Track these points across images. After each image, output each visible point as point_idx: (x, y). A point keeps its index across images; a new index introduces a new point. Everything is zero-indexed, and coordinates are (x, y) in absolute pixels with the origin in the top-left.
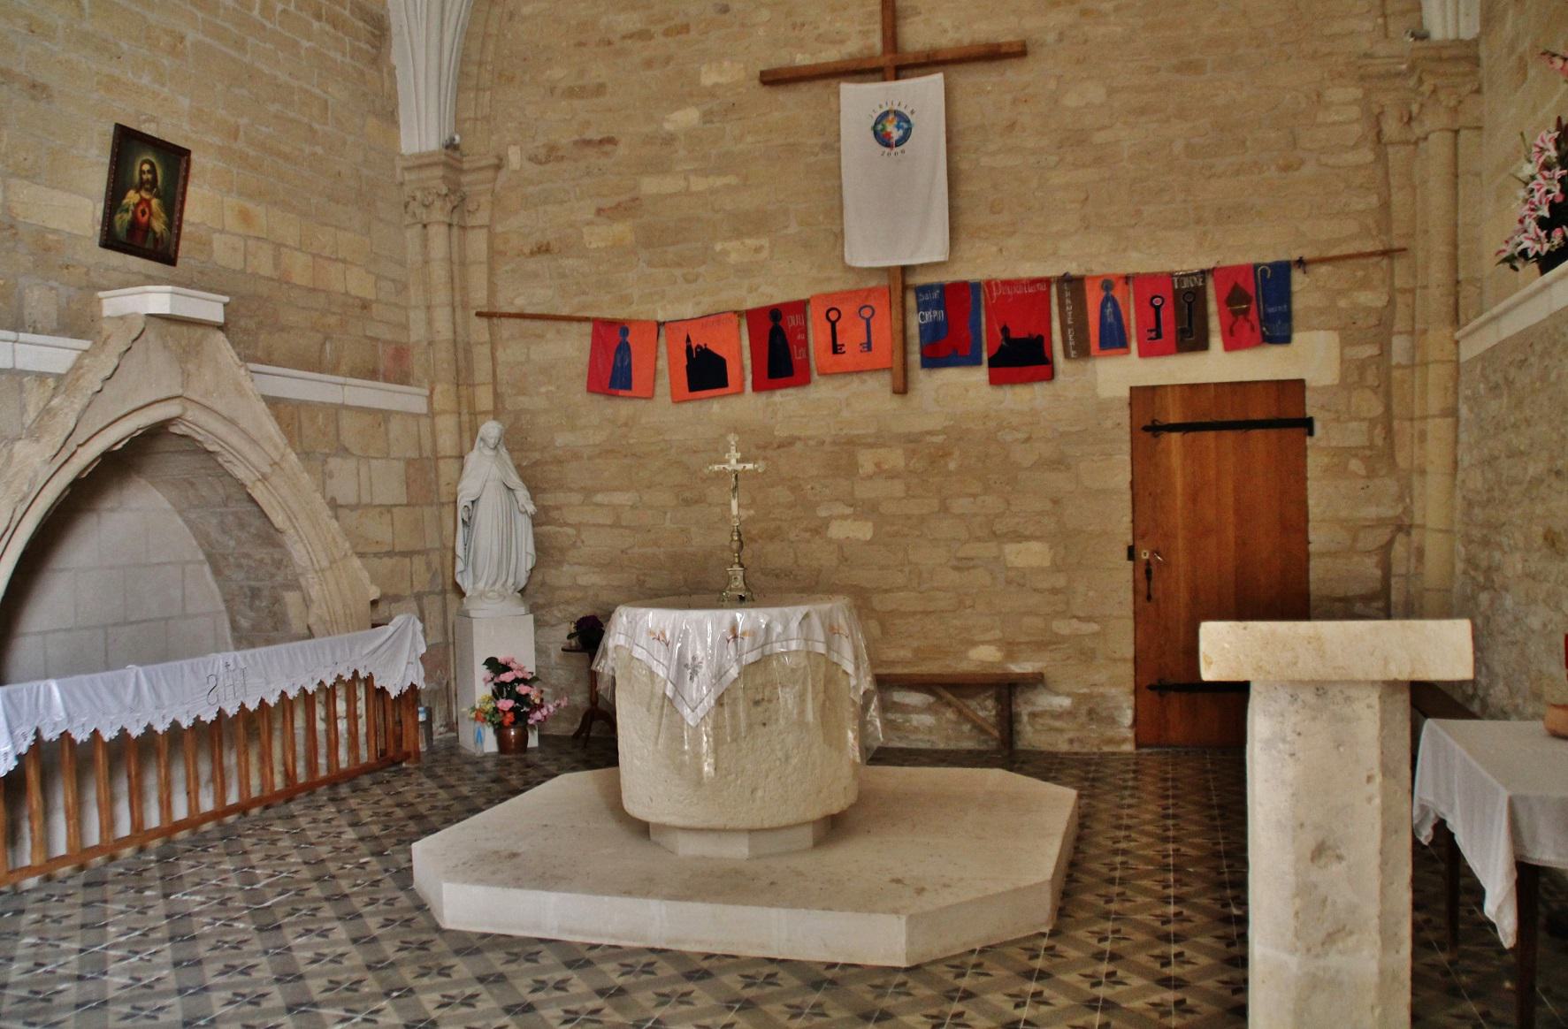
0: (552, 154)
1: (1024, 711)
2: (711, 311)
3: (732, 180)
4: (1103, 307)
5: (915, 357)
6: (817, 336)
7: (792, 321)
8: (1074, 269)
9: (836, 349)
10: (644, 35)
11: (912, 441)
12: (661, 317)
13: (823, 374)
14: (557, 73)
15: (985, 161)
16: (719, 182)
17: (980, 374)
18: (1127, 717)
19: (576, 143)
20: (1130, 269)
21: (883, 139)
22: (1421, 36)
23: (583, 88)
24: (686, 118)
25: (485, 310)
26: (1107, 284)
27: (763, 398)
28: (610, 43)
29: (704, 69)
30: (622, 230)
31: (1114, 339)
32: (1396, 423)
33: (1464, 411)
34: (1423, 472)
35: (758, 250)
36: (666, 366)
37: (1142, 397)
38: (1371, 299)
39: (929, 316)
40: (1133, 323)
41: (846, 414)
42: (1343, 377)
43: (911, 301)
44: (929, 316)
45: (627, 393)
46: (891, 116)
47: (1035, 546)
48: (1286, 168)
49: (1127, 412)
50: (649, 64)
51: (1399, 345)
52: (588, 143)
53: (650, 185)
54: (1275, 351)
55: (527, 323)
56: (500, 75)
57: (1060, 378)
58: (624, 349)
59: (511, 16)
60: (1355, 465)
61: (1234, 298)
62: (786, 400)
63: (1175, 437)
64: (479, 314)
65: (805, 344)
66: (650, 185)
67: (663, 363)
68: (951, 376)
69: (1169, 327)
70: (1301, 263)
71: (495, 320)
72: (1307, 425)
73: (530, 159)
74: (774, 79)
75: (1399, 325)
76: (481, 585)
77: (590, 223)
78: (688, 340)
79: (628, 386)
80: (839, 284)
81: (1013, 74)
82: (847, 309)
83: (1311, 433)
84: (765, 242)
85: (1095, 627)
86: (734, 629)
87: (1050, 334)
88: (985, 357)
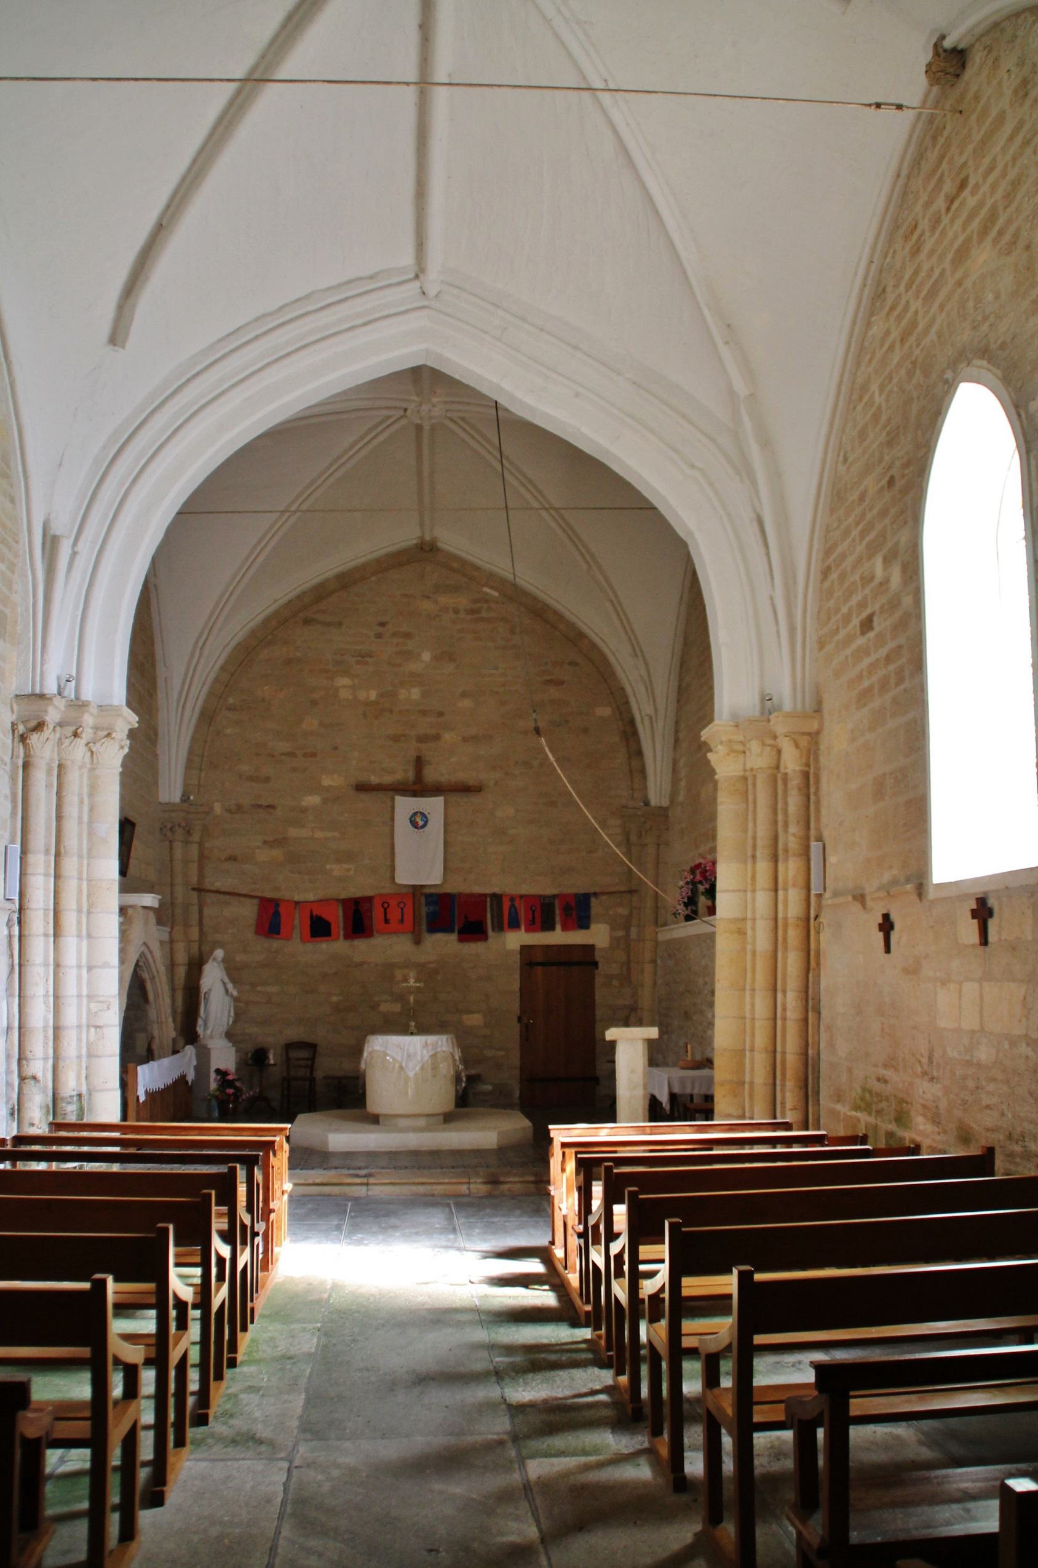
3: (337, 834)
4: (510, 908)
5: (424, 927)
6: (377, 913)
8: (497, 890)
9: (387, 921)
10: (292, 755)
11: (421, 967)
12: (297, 898)
13: (378, 932)
14: (245, 768)
16: (329, 834)
17: (454, 937)
18: (517, 1094)
20: (523, 892)
21: (414, 824)
22: (647, 803)
24: (313, 800)
25: (196, 886)
26: (512, 899)
27: (348, 943)
28: (273, 756)
29: (324, 777)
30: (277, 853)
31: (514, 925)
33: (659, 962)
34: (642, 986)
35: (348, 870)
36: (298, 923)
37: (525, 949)
38: (623, 911)
39: (432, 908)
40: (523, 913)
43: (423, 900)
44: (432, 908)
45: (278, 936)
46: (419, 814)
47: (476, 1016)
48: (590, 852)
49: (519, 956)
50: (294, 770)
51: (634, 931)
52: (260, 806)
53: (293, 832)
54: (583, 932)
55: (222, 896)
56: (211, 763)
57: (490, 940)
58: (277, 914)
60: (615, 982)
61: (567, 909)
63: (540, 968)
64: (194, 889)
65: (371, 917)
66: (293, 832)
67: (297, 922)
68: (440, 937)
69: (538, 920)
70: (595, 894)
71: (203, 893)
72: (595, 964)
73: (226, 810)
74: (362, 788)
75: (635, 921)
76: (209, 1032)
77: (258, 847)
78: (311, 912)
79: (278, 933)
80: (388, 889)
81: (475, 799)
83: (597, 968)
84: (351, 866)
86: (426, 1043)
87: (486, 919)
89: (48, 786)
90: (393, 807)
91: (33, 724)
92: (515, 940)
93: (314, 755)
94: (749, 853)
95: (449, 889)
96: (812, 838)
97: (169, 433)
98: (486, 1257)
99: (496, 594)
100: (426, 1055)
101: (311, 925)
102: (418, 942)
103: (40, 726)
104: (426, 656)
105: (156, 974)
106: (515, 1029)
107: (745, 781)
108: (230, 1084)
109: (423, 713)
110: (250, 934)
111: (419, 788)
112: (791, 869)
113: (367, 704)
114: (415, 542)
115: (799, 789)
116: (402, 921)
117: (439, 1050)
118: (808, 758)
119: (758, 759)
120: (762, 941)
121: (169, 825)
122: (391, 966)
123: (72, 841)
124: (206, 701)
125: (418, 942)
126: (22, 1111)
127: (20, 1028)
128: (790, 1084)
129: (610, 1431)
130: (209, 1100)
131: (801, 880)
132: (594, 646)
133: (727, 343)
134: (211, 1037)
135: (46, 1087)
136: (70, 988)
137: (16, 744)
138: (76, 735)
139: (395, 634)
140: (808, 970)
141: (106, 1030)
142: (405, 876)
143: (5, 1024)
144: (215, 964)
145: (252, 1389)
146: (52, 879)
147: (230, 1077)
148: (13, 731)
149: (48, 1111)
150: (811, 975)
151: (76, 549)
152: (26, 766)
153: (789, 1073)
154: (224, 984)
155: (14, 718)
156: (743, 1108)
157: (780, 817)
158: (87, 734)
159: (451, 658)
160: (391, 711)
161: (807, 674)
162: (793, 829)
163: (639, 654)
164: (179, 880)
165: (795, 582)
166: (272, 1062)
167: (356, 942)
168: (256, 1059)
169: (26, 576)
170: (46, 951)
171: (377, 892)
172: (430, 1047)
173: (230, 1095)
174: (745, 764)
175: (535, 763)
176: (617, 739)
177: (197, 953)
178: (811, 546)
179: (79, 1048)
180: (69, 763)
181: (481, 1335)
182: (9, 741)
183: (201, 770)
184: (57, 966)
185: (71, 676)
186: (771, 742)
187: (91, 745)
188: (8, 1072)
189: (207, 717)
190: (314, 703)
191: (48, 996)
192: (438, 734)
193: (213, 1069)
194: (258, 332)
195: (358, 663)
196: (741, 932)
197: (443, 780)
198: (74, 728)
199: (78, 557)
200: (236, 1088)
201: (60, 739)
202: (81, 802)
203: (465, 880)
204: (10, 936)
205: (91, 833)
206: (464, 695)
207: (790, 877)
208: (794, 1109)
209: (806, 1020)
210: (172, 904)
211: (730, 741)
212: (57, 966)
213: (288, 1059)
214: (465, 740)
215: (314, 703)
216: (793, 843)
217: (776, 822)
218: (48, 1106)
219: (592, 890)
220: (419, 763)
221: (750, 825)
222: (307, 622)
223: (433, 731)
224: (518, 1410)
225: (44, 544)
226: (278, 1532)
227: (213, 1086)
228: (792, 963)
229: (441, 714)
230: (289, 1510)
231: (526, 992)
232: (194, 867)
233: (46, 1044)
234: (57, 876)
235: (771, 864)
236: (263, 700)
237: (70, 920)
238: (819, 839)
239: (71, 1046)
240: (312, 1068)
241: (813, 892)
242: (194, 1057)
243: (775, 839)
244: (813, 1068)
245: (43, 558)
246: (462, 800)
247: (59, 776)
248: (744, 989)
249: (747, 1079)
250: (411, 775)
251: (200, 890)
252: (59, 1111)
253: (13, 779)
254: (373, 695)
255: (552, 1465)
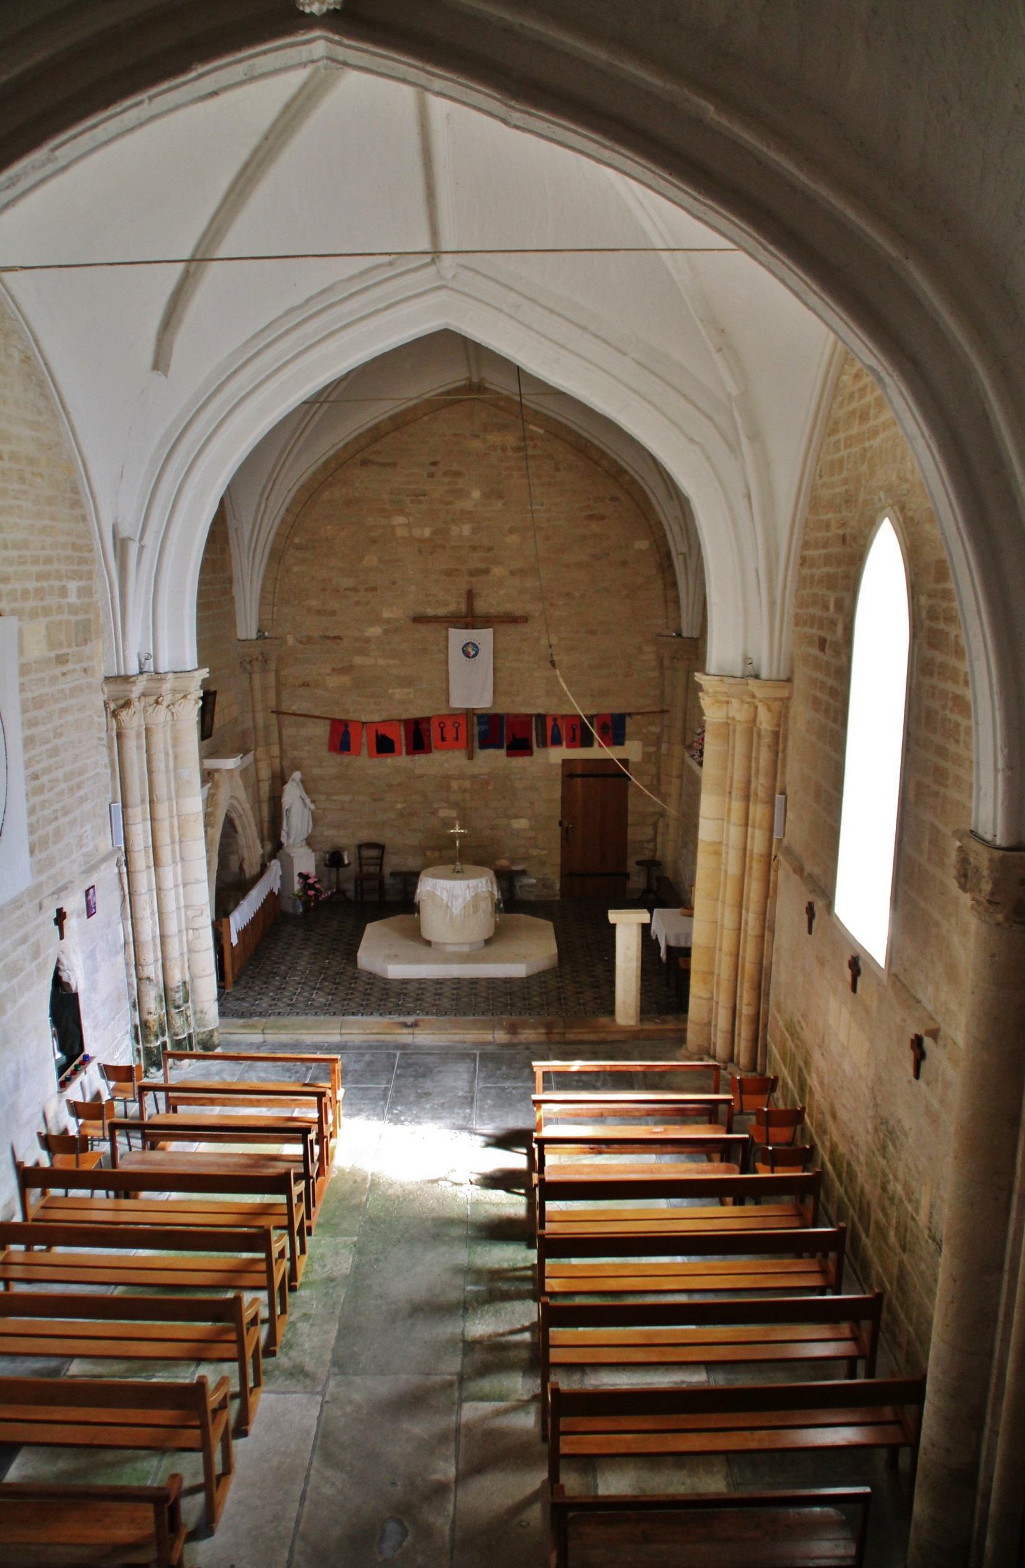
0: (310, 640)
1: (518, 884)
2: (387, 719)
4: (553, 728)
5: (476, 744)
6: (435, 733)
7: (424, 726)
8: (541, 711)
9: (443, 739)
10: (355, 590)
11: (473, 778)
12: (364, 719)
13: (437, 748)
14: (313, 603)
15: (507, 664)
16: (391, 662)
17: (503, 752)
18: (558, 886)
19: (321, 637)
20: (564, 712)
21: (466, 654)
22: (679, 635)
23: (325, 611)
24: (375, 631)
26: (555, 719)
27: (409, 758)
28: (338, 591)
30: (345, 680)
31: (556, 742)
32: (662, 776)
34: (670, 796)
35: (408, 694)
36: (365, 740)
37: (566, 763)
38: (655, 729)
39: (483, 728)
41: (446, 765)
42: (643, 759)
43: (475, 720)
44: (483, 728)
50: (357, 603)
51: (664, 746)
52: (327, 638)
53: (358, 660)
55: (298, 718)
57: (535, 754)
59: (287, 571)
62: (421, 759)
63: (579, 779)
64: (273, 712)
65: (430, 736)
66: (358, 660)
67: (364, 740)
70: (630, 714)
74: (420, 619)
75: (665, 738)
76: (291, 841)
77: (328, 675)
78: (377, 731)
80: (444, 712)
82: (449, 723)
84: (411, 690)
85: (546, 852)
88: (505, 746)
89: (139, 748)
90: (447, 637)
91: (121, 702)
92: (558, 754)
93: (374, 589)
94: (728, 790)
95: (498, 710)
96: (778, 790)
97: (214, 426)
98: (488, 1145)
99: (542, 432)
100: (469, 895)
101: (377, 743)
102: (471, 756)
103: (127, 704)
104: (476, 494)
105: (242, 812)
106: (557, 832)
107: (727, 726)
108: (312, 887)
109: (474, 548)
110: (324, 752)
111: (470, 620)
112: (758, 811)
113: (421, 541)
114: (463, 383)
115: (769, 747)
116: (457, 739)
117: (479, 891)
118: (779, 719)
119: (738, 712)
120: (732, 867)
121: (248, 659)
122: (448, 778)
123: (162, 791)
124: (274, 542)
125: (471, 756)
126: (142, 1003)
127: (134, 941)
128: (746, 985)
129: (521, 1374)
130: (295, 900)
131: (765, 824)
132: (634, 482)
133: (720, 350)
134: (294, 846)
135: (158, 982)
136: (171, 905)
137: (109, 719)
138: (157, 702)
139: (445, 474)
140: (767, 896)
141: (201, 932)
142: (458, 702)
143: (122, 941)
144: (294, 784)
145: (306, 1317)
146: (149, 822)
147: (311, 881)
148: (106, 708)
149: (161, 1000)
150: (769, 901)
151: (143, 543)
152: (119, 736)
153: (747, 976)
154: (303, 800)
155: (105, 697)
156: (712, 993)
157: (753, 765)
158: (167, 700)
159: (500, 496)
160: (444, 548)
161: (783, 643)
162: (762, 780)
163: (674, 496)
164: (259, 707)
165: (778, 560)
166: (346, 862)
167: (417, 757)
168: (334, 859)
169: (103, 576)
170: (149, 880)
171: (435, 713)
172: (472, 890)
173: (311, 896)
174: (727, 714)
175: (577, 594)
176: (654, 571)
177: (279, 769)
178: (792, 533)
179: (181, 948)
180: (154, 726)
181: (462, 1256)
182: (104, 719)
183: (274, 606)
184: (159, 889)
185: (149, 654)
186: (749, 700)
187: (171, 707)
188: (128, 976)
189: (276, 556)
190: (374, 541)
191: (152, 890)
192: (488, 568)
193: (296, 873)
194: (288, 326)
195: (412, 501)
196: (718, 853)
197: (492, 611)
198: (155, 697)
199: (145, 550)
200: (317, 890)
201: (145, 707)
202: (167, 754)
203: (512, 701)
204: (120, 874)
205: (177, 777)
206: (511, 531)
207: (758, 819)
208: (748, 1005)
209: (762, 936)
210: (255, 728)
211: (716, 692)
212: (159, 889)
213: (360, 858)
214: (512, 573)
215: (374, 541)
216: (762, 793)
217: (750, 767)
218: (161, 996)
219: (628, 710)
220: (470, 596)
221: (729, 765)
222: (364, 463)
223: (482, 566)
224: (470, 1346)
225: (115, 544)
226: (311, 1464)
227: (297, 887)
228: (754, 890)
229: (490, 549)
230: (319, 1443)
231: (567, 800)
232: (272, 694)
233: (155, 951)
234: (153, 819)
235: (743, 804)
236: (327, 539)
237: (166, 853)
238: (783, 793)
239: (175, 948)
240: (381, 865)
241: (775, 836)
242: (279, 869)
243: (748, 782)
244: (766, 974)
245: (115, 557)
246: (511, 629)
247: (147, 737)
248: (717, 900)
249: (716, 972)
250: (463, 608)
251: (278, 712)
252: (169, 998)
253: (110, 748)
254: (427, 532)
255: (477, 1409)
